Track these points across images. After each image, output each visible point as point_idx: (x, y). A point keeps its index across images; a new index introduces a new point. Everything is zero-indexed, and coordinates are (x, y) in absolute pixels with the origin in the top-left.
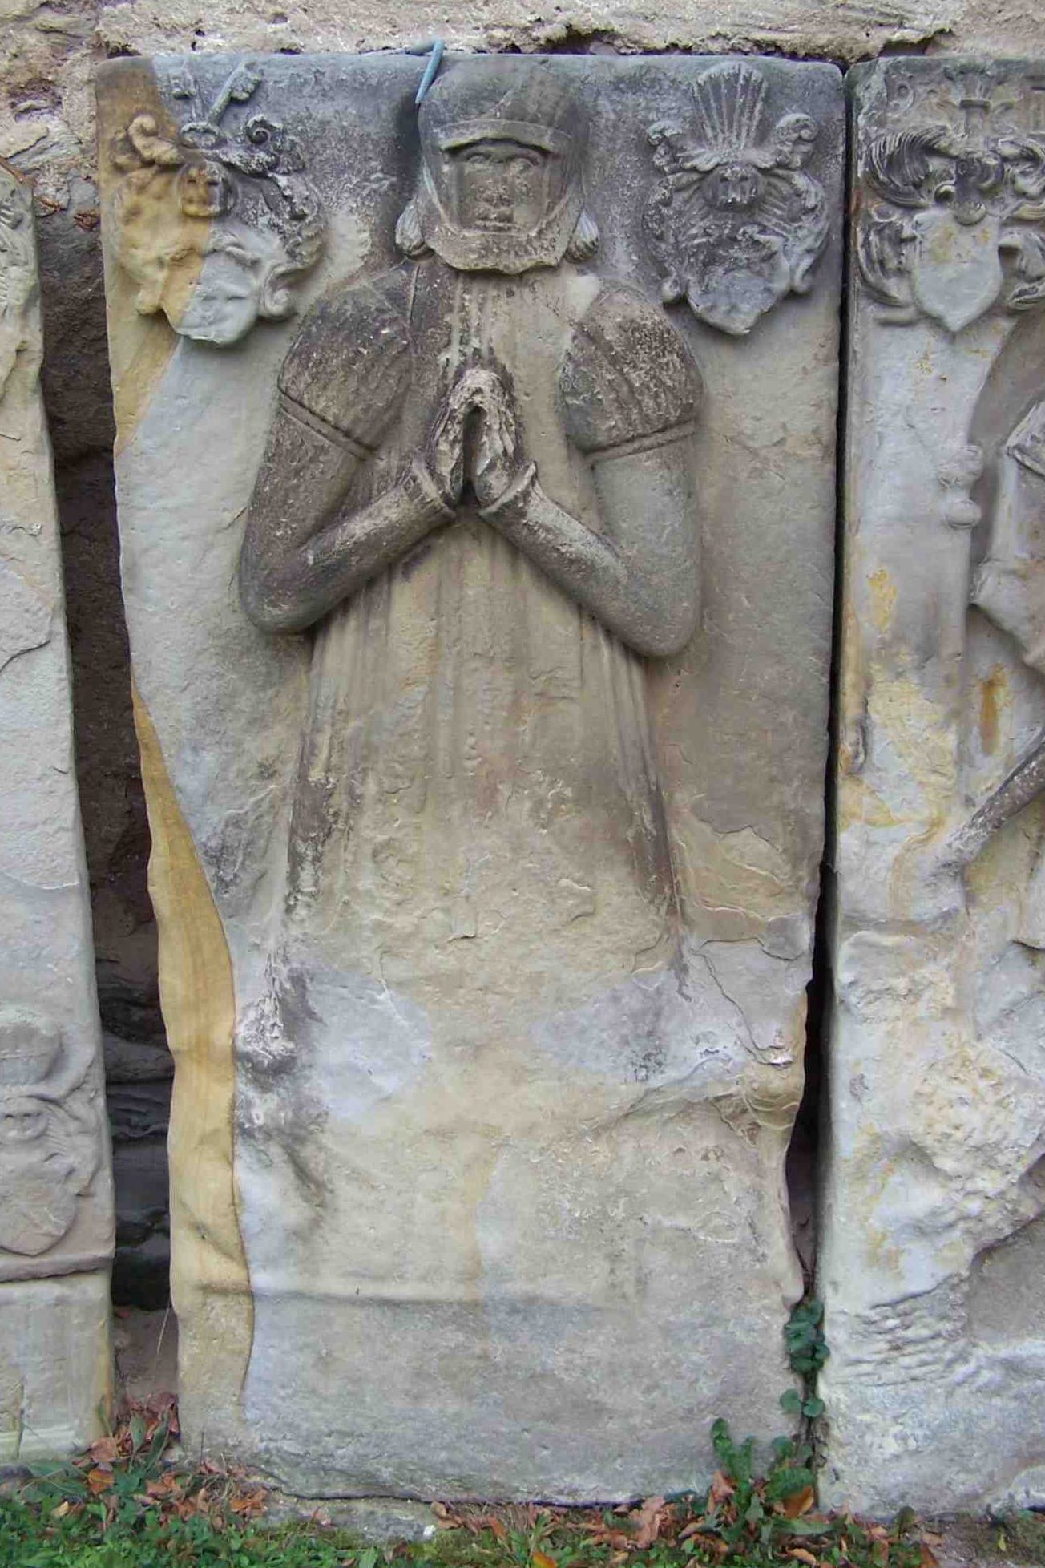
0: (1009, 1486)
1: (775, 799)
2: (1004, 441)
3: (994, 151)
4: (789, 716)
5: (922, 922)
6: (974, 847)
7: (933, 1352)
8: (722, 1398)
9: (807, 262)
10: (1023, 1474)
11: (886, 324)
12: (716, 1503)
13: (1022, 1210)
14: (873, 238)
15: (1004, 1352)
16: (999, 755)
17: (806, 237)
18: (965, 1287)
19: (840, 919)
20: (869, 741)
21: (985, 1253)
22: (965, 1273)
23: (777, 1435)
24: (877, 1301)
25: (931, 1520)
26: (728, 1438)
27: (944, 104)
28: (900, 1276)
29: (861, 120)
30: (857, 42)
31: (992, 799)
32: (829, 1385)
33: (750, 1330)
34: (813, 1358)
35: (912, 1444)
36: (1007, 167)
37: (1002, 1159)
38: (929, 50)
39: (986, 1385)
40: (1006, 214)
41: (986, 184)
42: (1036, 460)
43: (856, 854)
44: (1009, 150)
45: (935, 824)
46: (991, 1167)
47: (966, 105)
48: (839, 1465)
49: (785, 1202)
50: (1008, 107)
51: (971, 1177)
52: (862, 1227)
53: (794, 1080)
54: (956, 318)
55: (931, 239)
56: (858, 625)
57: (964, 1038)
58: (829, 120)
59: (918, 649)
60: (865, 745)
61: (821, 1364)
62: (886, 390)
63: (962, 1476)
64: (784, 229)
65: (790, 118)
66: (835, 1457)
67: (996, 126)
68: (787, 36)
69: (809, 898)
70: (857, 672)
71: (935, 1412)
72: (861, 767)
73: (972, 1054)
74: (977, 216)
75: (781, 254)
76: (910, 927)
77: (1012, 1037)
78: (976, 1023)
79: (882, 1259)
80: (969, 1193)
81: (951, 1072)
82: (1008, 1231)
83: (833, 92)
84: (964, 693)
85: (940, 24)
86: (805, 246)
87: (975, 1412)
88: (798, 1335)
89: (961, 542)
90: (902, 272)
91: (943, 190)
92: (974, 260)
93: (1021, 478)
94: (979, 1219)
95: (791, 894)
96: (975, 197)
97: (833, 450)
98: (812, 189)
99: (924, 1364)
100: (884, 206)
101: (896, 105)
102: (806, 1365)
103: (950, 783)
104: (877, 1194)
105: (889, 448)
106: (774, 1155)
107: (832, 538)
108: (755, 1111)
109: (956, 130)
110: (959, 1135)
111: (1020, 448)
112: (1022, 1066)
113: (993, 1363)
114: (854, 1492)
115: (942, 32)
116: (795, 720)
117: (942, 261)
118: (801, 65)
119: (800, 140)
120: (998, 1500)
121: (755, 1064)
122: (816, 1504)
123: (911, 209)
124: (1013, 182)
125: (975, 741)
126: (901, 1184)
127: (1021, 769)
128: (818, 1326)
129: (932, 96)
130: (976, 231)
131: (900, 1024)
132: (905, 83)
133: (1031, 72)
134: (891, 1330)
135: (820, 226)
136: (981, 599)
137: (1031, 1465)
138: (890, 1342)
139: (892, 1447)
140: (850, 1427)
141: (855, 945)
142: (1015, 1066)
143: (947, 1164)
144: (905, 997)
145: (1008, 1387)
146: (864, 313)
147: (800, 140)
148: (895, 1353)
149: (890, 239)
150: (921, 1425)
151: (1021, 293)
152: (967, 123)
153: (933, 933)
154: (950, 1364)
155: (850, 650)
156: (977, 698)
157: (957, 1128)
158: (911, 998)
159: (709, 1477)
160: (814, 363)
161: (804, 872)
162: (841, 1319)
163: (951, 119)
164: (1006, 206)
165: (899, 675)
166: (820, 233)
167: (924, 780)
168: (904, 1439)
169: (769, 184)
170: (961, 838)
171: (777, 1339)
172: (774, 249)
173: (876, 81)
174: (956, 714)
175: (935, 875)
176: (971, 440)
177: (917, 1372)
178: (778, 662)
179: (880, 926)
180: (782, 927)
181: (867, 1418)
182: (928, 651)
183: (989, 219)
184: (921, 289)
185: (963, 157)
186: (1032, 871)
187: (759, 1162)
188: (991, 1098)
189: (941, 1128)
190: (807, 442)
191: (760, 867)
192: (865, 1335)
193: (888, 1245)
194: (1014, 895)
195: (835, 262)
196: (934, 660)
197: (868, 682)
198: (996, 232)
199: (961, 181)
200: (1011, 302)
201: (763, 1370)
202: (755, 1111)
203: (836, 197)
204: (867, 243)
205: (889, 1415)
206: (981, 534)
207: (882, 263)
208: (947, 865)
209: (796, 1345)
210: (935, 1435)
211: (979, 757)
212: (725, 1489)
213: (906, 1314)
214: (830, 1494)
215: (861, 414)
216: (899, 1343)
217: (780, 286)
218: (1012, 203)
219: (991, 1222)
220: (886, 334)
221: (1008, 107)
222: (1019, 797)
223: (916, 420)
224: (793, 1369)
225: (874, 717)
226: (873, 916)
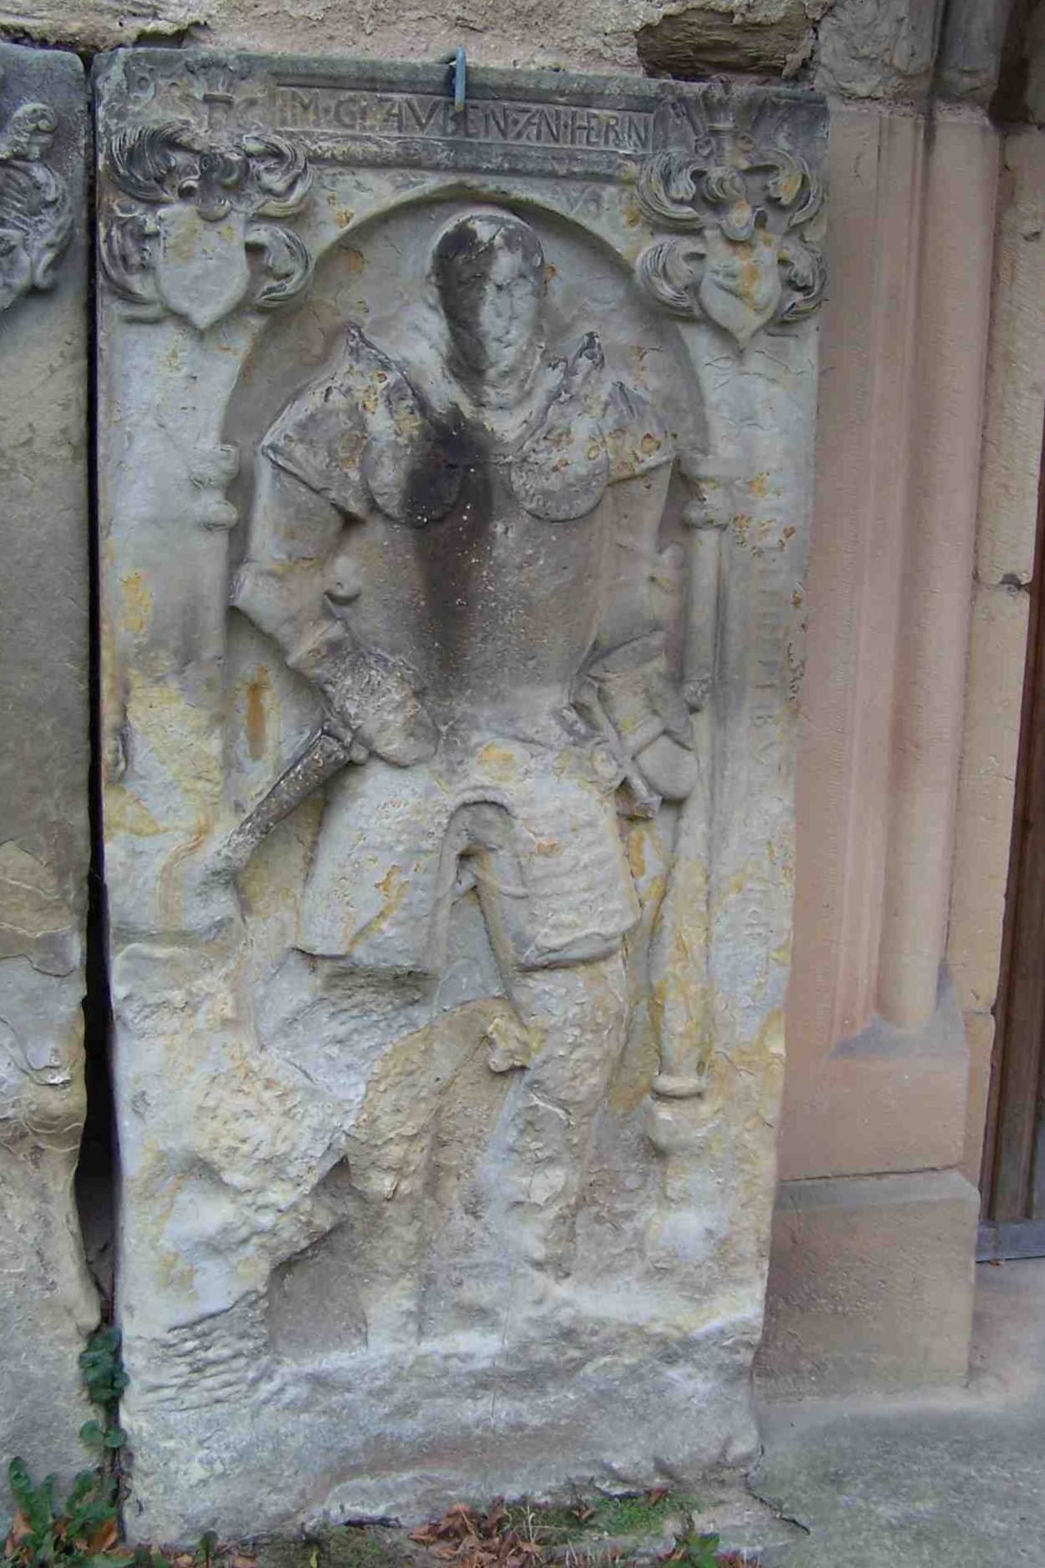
0: (322, 1503)
1: (37, 811)
2: (260, 440)
3: (238, 146)
4: (47, 726)
5: (195, 932)
6: (244, 853)
7: (236, 1371)
8: (18, 1434)
9: (49, 256)
10: (337, 1489)
11: (132, 321)
12: (15, 1547)
13: (317, 1221)
14: (115, 232)
15: (310, 1366)
16: (269, 758)
17: (47, 231)
18: (264, 1304)
19: (112, 931)
20: (130, 747)
21: (285, 1267)
22: (263, 1289)
23: (77, 1470)
24: (174, 1324)
25: (245, 1544)
26: (26, 1477)
27: (187, 98)
28: (195, 1296)
29: (101, 112)
30: (110, 31)
31: (261, 804)
32: (130, 1414)
33: (43, 1362)
34: (112, 1388)
35: (219, 1468)
36: (252, 163)
37: (292, 1171)
38: (185, 43)
39: (292, 1402)
40: (251, 212)
41: (229, 181)
42: (290, 459)
43: (121, 864)
44: (253, 147)
45: (203, 832)
46: (282, 1180)
47: (208, 100)
48: (144, 1495)
49: (74, 1226)
50: (252, 103)
51: (261, 1190)
52: (154, 1248)
53: (73, 1101)
54: (203, 316)
55: (175, 234)
56: (112, 632)
57: (247, 1048)
58: (70, 111)
59: (176, 653)
60: (125, 752)
61: (121, 1391)
62: (136, 384)
63: (274, 1497)
64: (24, 222)
65: (28, 107)
66: (139, 1488)
67: (241, 122)
68: (36, 23)
69: (76, 911)
70: (113, 677)
71: (240, 1433)
72: (123, 774)
73: (255, 1064)
74: (221, 213)
75: (20, 249)
76: (183, 937)
77: (297, 1046)
78: (258, 1033)
79: (177, 1279)
80: (259, 1208)
81: (234, 1084)
82: (304, 1244)
83: (74, 83)
84: (228, 697)
85: (196, 16)
86: (45, 241)
87: (282, 1430)
88: (94, 1364)
89: (220, 541)
90: (145, 268)
91: (184, 185)
92: (221, 257)
93: (275, 477)
94: (273, 1232)
95: (58, 908)
96: (219, 192)
97: (84, 451)
98: (53, 182)
99: (229, 1384)
100: (127, 201)
101: (137, 97)
102: (105, 1394)
103: (217, 789)
104: (165, 1215)
105: (141, 445)
106: (60, 1181)
107: (85, 540)
108: (36, 1134)
109: (200, 124)
110: (246, 1148)
111: (273, 447)
112: (307, 1076)
113: (297, 1379)
114: (162, 1521)
115: (196, 24)
116: (53, 727)
117: (189, 258)
118: (49, 53)
119: (37, 131)
120: (312, 1518)
121: (32, 1085)
122: (123, 1537)
123: (155, 204)
124: (259, 179)
125: (242, 747)
126: (191, 1201)
127: (287, 773)
128: (116, 1354)
129: (173, 89)
130: (222, 227)
131: (179, 1039)
132: (147, 75)
133: (276, 68)
134: (189, 1353)
135: (61, 220)
136: (239, 603)
137: (345, 1480)
138: (190, 1364)
139: (198, 1472)
140: (153, 1456)
141: (128, 958)
142: (299, 1076)
143: (235, 1178)
144: (182, 1009)
145: (317, 1402)
146: (110, 310)
147: (37, 131)
148: (195, 1376)
149: (132, 235)
150: (227, 1448)
151: (271, 290)
152: (210, 117)
153: (207, 943)
154: (255, 1382)
155: (106, 655)
156: (243, 702)
157: (244, 1141)
158: (188, 1011)
159: (10, 1519)
160: (60, 360)
161: (70, 885)
162: (139, 1344)
163: (194, 113)
164: (253, 202)
165: (158, 680)
166: (60, 229)
167: (189, 787)
168: (210, 1463)
169: (8, 176)
170: (229, 845)
171: (72, 1369)
172: (13, 243)
173: (116, 72)
174: (220, 719)
175: (205, 884)
176: (225, 439)
177: (221, 1393)
178: (35, 670)
179: (152, 938)
180: (52, 943)
181: (171, 1444)
182: (187, 656)
183: (234, 214)
184: (165, 285)
185: (206, 152)
186: (308, 877)
187: (44, 1186)
188: (276, 1108)
189: (226, 1142)
190: (54, 442)
191: (25, 881)
192: (164, 1360)
193: (181, 1265)
194: (290, 901)
195: (79, 260)
196: (193, 663)
197: (126, 689)
198: (241, 229)
199: (204, 177)
200: (260, 300)
201: (61, 1403)
202: (36, 1134)
203: (80, 191)
204: (109, 237)
205: (193, 1440)
206: (238, 535)
207: (124, 259)
208: (216, 873)
209: (93, 1375)
210: (242, 1456)
211: (248, 764)
212: (23, 1530)
213: (204, 1334)
214: (137, 1527)
215: (110, 410)
216: (201, 1364)
217: (20, 281)
218: (259, 199)
219: (285, 1235)
220: (133, 332)
221: (252, 103)
222: (287, 802)
223: (166, 420)
224: (92, 1400)
225: (135, 725)
226: (145, 928)
